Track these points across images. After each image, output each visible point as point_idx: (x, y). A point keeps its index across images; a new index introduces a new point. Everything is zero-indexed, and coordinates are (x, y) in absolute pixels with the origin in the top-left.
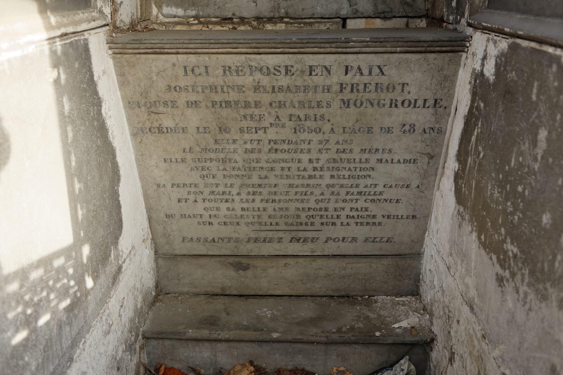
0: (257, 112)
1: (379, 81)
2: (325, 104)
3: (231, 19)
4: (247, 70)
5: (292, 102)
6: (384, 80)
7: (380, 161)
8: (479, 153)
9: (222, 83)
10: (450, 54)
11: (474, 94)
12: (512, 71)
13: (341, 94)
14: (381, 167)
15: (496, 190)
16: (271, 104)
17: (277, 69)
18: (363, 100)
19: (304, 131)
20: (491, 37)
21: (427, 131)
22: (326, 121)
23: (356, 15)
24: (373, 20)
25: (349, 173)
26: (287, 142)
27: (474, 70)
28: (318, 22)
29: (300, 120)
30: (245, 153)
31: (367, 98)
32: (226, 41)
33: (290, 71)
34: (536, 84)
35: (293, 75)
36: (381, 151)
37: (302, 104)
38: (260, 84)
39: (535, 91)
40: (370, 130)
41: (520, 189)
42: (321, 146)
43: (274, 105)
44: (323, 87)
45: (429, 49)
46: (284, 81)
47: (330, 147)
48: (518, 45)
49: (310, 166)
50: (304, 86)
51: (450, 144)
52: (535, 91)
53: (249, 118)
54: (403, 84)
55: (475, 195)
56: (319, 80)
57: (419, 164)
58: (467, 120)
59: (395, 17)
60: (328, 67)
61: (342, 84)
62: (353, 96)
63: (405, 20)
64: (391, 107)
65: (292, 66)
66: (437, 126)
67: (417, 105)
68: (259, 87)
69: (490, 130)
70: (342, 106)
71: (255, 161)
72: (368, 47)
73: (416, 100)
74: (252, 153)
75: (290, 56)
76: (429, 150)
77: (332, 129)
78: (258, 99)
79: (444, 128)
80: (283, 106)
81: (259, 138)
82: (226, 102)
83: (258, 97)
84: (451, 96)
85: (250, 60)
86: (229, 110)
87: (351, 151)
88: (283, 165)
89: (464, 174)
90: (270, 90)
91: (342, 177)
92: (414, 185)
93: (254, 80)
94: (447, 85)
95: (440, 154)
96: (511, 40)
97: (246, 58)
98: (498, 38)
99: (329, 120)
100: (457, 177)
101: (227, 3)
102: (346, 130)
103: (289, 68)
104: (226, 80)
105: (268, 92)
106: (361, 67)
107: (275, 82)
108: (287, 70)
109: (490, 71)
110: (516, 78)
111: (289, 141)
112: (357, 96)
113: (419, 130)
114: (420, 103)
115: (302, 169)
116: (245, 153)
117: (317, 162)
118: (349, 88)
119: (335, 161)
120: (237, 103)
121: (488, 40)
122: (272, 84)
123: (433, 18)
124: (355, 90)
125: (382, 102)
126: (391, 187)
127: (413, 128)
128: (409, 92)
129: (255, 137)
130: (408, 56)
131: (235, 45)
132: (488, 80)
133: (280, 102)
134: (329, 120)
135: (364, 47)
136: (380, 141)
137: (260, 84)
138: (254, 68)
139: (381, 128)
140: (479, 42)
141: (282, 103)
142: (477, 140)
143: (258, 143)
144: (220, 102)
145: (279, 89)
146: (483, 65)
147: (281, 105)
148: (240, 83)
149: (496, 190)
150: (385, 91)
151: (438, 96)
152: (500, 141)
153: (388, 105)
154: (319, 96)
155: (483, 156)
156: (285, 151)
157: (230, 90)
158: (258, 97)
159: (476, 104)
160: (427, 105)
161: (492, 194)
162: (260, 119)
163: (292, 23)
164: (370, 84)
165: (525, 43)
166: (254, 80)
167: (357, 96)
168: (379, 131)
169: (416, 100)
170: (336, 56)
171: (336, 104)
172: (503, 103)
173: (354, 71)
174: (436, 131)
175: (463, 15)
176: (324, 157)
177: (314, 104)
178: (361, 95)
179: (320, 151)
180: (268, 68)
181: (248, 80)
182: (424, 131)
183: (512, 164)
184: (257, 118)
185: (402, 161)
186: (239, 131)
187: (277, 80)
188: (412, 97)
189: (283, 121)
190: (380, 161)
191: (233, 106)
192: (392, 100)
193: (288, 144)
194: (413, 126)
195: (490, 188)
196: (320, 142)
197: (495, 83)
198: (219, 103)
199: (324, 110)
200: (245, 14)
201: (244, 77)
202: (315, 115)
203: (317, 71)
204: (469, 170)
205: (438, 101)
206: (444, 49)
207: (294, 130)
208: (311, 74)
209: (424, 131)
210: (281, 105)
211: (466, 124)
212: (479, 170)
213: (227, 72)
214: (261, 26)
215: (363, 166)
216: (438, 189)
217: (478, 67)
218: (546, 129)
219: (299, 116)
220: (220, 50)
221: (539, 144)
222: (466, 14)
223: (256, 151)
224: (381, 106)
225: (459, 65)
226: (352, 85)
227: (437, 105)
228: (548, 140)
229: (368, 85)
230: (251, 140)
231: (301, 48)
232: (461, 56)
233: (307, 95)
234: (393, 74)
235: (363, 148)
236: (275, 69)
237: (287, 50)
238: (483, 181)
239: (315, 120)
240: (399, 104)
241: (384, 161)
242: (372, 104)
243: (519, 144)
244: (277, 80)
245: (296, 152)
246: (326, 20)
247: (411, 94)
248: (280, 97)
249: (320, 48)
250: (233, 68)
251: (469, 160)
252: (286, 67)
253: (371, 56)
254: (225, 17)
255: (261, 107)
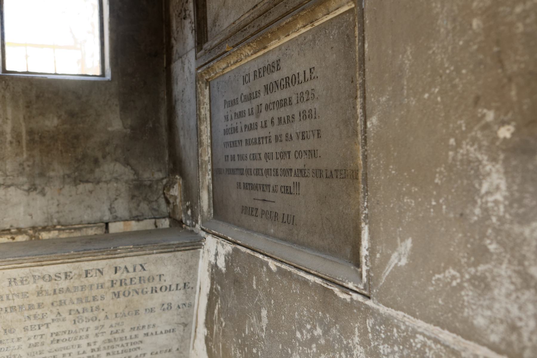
0: (40, 312)
1: (142, 275)
2: (99, 298)
3: (9, 230)
4: (31, 280)
5: (71, 299)
6: (145, 274)
7: (147, 335)
8: (222, 323)
9: (8, 292)
10: (192, 251)
11: (212, 279)
12: (237, 267)
13: (112, 288)
14: (148, 340)
15: (238, 351)
16: (52, 304)
17: (58, 276)
18: (130, 290)
19: (83, 321)
20: (219, 241)
21: (181, 306)
22: (101, 310)
23: (116, 219)
24: (129, 222)
25: (122, 348)
26: (67, 332)
27: (210, 262)
28: (86, 227)
29: (79, 313)
30: (29, 347)
31: (133, 288)
32: (12, 259)
33: (69, 276)
34: (254, 277)
35: (72, 278)
36: (146, 327)
37: (80, 300)
38: (43, 289)
39: (254, 282)
40: (137, 312)
41: (254, 351)
42: (97, 331)
43: (55, 304)
44: (98, 285)
45: (176, 249)
46: (64, 284)
47: (105, 330)
48: (238, 250)
49: (89, 349)
50: (82, 286)
51: (199, 314)
52: (254, 282)
53: (32, 318)
54: (160, 276)
55: (223, 355)
56: (93, 280)
57: (177, 332)
58: (209, 297)
59: (146, 219)
60: (101, 270)
61: (112, 281)
62: (122, 289)
63: (153, 220)
64: (152, 292)
65: (71, 272)
66: (188, 302)
67: (172, 289)
68: (42, 291)
69: (228, 306)
70: (114, 297)
71: (38, 353)
72: (132, 251)
73: (170, 286)
74: (35, 346)
75: (69, 264)
76: (183, 320)
77: (106, 316)
78: (41, 301)
79: (192, 303)
80: (63, 304)
81: (42, 333)
82: (11, 307)
83: (40, 300)
84: (196, 280)
85: (34, 271)
86: (14, 313)
87: (123, 331)
88: (64, 352)
89: (212, 337)
90: (52, 292)
91: (116, 353)
92: (174, 349)
93: (37, 286)
94: (192, 272)
95: (191, 322)
96: (233, 246)
97: (30, 270)
98: (224, 243)
99: (103, 310)
100: (207, 340)
101: (5, 218)
102: (118, 315)
103: (68, 274)
104: (12, 290)
105: (50, 295)
106: (127, 267)
107: (56, 285)
108: (67, 276)
109: (221, 264)
110: (240, 272)
111: (69, 331)
112: (125, 288)
113: (174, 307)
114: (173, 287)
115: (81, 352)
116: (29, 347)
117: (95, 345)
118: (118, 283)
119: (110, 341)
120: (21, 307)
121: (217, 243)
122: (54, 288)
123: (174, 219)
124: (123, 284)
125: (145, 290)
126: (157, 353)
127: (170, 306)
128: (165, 281)
129: (38, 332)
130: (162, 255)
131: (20, 261)
132: (221, 270)
133: (60, 301)
134: (103, 310)
135: (129, 252)
136: (145, 319)
137: (43, 289)
138: (37, 277)
139: (146, 310)
140: (210, 242)
141: (63, 301)
142: (219, 313)
143: (42, 337)
144: (6, 308)
145: (60, 291)
146: (216, 259)
147: (62, 303)
148: (24, 290)
149: (238, 351)
150: (147, 281)
151: (186, 281)
152: (236, 315)
153: (150, 292)
154: (95, 292)
155: (225, 325)
156: (66, 340)
157: (15, 297)
158: (40, 300)
159: (214, 287)
160: (179, 288)
161: (235, 354)
162: (43, 317)
163: (63, 230)
164: (135, 278)
165: (243, 249)
166: (37, 286)
167: (125, 288)
168: (144, 311)
169: (170, 286)
170: (107, 261)
171: (109, 297)
172: (234, 288)
173: (122, 270)
174: (187, 305)
175: (197, 222)
176: (100, 339)
177: (90, 299)
178: (128, 287)
179: (97, 335)
180: (50, 276)
181: (32, 287)
182: (179, 307)
183: (247, 333)
184: (40, 316)
185: (164, 332)
186: (23, 330)
187: (57, 284)
188: (167, 284)
189: (64, 315)
190: (147, 335)
191: (18, 310)
192: (152, 288)
193: (69, 333)
194: (170, 305)
195: (233, 349)
196: (97, 328)
197: (226, 274)
198: (4, 309)
199: (98, 303)
200: (22, 225)
201: (28, 285)
202: (92, 307)
203: (91, 274)
204: (216, 335)
205: (187, 284)
206: (187, 248)
207: (73, 322)
208: (87, 276)
209: (179, 307)
210: (62, 303)
211: (209, 300)
212: (223, 336)
213: (13, 283)
214: (37, 234)
215: (133, 341)
216: (193, 348)
217: (213, 261)
218: (266, 309)
219: (77, 310)
220: (7, 267)
221: (263, 319)
222: (200, 222)
223: (40, 344)
224: (144, 293)
225: (199, 257)
226: (121, 281)
227: (186, 287)
228: (268, 317)
229: (133, 279)
230: (35, 336)
231: (79, 258)
232: (199, 251)
233: (84, 293)
234: (152, 269)
235: (132, 327)
236: (56, 276)
237: (67, 260)
238: (228, 344)
239: (92, 311)
240: (158, 290)
241: (149, 334)
242: (137, 293)
243: (249, 318)
244: (57, 284)
245: (75, 339)
246: (92, 225)
247: (167, 282)
248: (61, 297)
249: (94, 256)
250: (18, 279)
251: (215, 327)
252: (66, 273)
253: (135, 258)
254: (3, 229)
255: (43, 308)
